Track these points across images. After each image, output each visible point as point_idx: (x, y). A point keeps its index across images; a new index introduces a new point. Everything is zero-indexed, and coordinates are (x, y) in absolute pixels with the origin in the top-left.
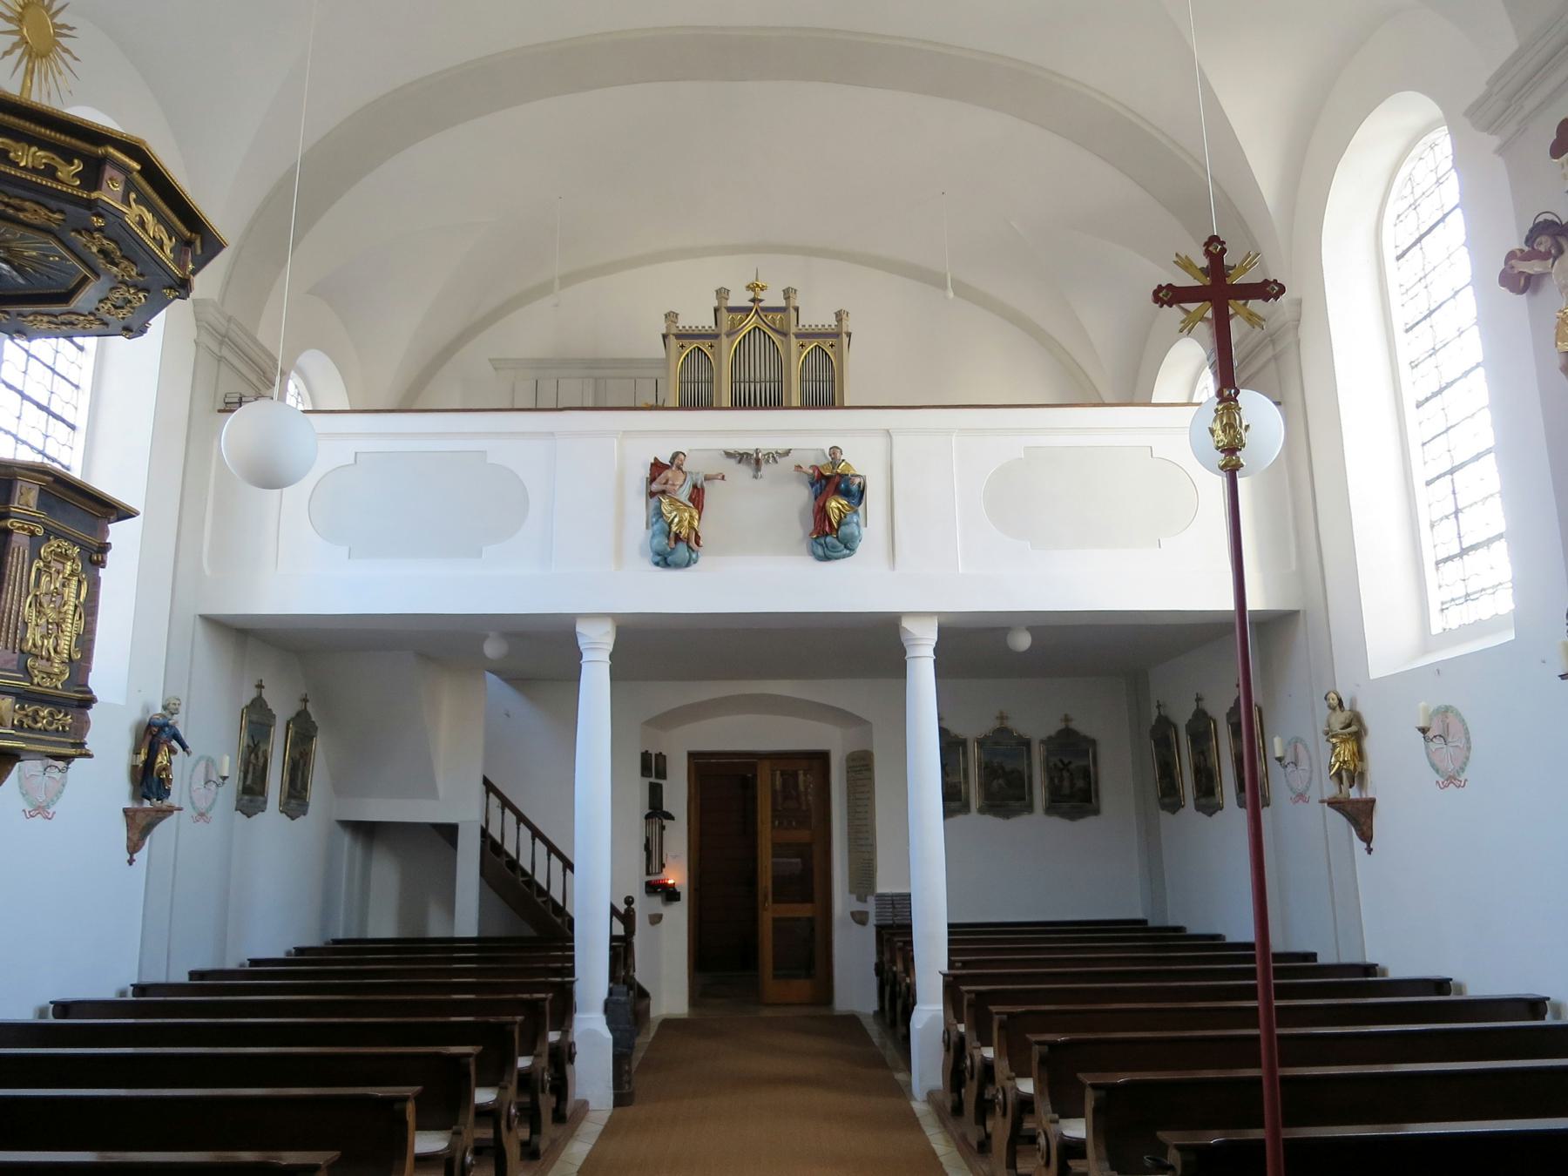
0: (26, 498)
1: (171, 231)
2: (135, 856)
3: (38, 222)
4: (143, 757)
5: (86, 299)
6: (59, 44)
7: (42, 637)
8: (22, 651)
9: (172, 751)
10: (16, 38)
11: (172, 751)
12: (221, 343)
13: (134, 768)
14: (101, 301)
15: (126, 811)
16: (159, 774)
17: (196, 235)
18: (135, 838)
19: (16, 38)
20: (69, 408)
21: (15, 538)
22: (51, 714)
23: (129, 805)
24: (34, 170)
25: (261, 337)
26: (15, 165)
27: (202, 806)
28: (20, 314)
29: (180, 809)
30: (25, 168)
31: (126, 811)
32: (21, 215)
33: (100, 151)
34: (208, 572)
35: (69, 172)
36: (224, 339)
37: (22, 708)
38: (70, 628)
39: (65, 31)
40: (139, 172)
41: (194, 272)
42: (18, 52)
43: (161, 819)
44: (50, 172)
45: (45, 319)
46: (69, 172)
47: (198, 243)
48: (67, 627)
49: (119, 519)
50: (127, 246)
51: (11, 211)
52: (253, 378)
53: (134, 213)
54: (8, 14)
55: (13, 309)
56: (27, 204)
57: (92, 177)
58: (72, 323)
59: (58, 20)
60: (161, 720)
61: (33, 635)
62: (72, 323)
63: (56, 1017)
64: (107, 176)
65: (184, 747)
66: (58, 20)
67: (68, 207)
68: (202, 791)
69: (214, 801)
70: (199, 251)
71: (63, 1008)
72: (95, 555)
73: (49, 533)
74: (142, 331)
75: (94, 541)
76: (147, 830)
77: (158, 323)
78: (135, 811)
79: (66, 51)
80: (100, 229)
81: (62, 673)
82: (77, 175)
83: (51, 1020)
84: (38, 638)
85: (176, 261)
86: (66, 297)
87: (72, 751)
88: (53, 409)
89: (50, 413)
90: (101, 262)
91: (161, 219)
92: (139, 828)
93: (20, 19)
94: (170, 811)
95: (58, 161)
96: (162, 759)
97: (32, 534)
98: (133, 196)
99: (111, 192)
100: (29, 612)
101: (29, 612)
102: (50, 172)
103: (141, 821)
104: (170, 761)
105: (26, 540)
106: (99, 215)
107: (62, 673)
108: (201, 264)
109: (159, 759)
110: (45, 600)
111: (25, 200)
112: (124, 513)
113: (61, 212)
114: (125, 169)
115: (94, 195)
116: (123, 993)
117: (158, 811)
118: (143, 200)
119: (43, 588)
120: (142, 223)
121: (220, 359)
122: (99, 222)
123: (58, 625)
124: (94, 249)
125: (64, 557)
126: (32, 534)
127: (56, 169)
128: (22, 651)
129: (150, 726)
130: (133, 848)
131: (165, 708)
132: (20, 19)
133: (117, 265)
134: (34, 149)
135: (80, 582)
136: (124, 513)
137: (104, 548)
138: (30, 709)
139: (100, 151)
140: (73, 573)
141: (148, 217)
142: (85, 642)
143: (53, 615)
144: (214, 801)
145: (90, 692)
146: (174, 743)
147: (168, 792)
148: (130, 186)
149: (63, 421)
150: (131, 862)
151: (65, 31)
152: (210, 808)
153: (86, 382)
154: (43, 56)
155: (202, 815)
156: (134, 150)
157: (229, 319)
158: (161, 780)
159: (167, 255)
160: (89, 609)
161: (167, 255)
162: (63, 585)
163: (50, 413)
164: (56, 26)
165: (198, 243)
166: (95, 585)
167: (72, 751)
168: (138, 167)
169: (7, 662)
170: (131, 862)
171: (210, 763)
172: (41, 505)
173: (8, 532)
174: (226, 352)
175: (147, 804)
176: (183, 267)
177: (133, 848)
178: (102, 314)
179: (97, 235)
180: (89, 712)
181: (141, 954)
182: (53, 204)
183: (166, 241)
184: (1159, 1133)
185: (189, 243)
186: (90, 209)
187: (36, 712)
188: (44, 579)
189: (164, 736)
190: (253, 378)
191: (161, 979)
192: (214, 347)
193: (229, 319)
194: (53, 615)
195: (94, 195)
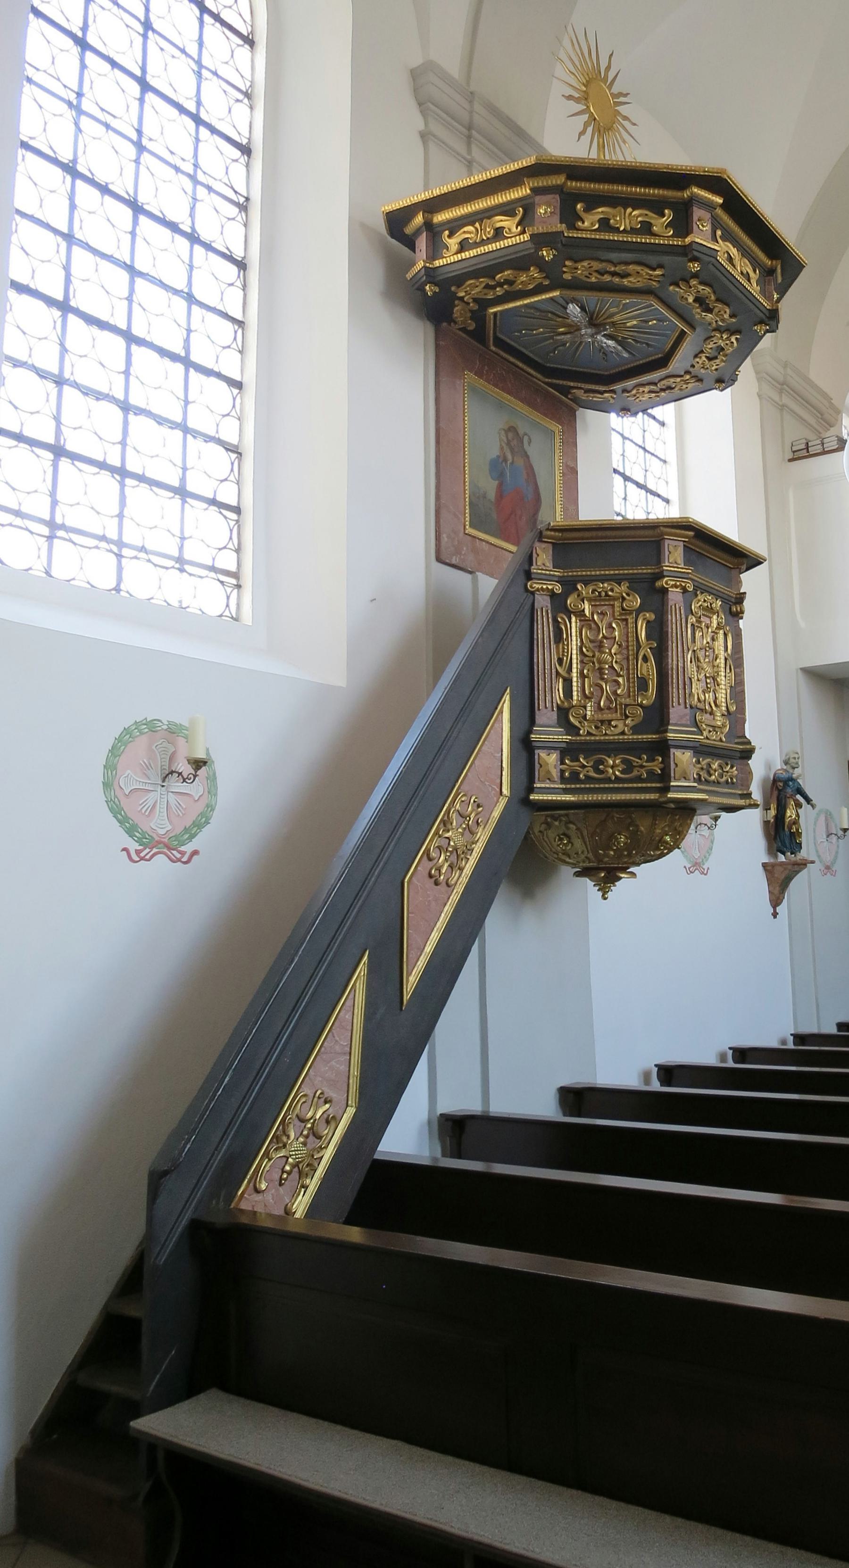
0: (674, 556)
1: (755, 263)
2: (778, 909)
3: (639, 285)
4: (773, 812)
5: (677, 364)
6: (618, 113)
7: (704, 692)
8: (691, 707)
9: (798, 805)
10: (585, 117)
11: (798, 805)
12: (781, 392)
13: (766, 823)
14: (696, 356)
15: (764, 865)
16: (790, 828)
17: (777, 258)
18: (776, 891)
19: (585, 117)
20: (662, 483)
21: (671, 596)
22: (720, 766)
23: (766, 859)
24: (633, 231)
25: (813, 376)
26: (617, 230)
27: (828, 858)
28: (625, 391)
29: (813, 862)
30: (624, 231)
31: (764, 865)
32: (625, 282)
33: (686, 194)
34: (802, 624)
35: (661, 223)
36: (782, 386)
37: (698, 762)
38: (724, 680)
39: (622, 99)
40: (722, 206)
41: (779, 300)
42: (590, 130)
43: (797, 872)
44: (646, 228)
45: (646, 389)
46: (661, 223)
47: (779, 271)
48: (722, 679)
49: (748, 569)
50: (725, 290)
51: (617, 280)
52: (812, 421)
53: (723, 248)
54: (577, 95)
55: (618, 387)
56: (632, 268)
57: (682, 225)
58: (670, 388)
59: (615, 89)
60: (785, 775)
61: (697, 688)
62: (670, 388)
63: (735, 1062)
64: (695, 218)
65: (808, 800)
66: (615, 89)
67: (666, 259)
68: (826, 843)
69: (837, 853)
70: (780, 280)
71: (741, 1054)
72: (734, 606)
73: (699, 588)
74: (733, 380)
75: (731, 592)
76: (785, 884)
77: (746, 369)
78: (773, 865)
79: (626, 118)
80: (695, 276)
81: (724, 726)
82: (669, 225)
83: (730, 1064)
84: (700, 692)
85: (763, 292)
86: (663, 362)
87: (741, 802)
88: (651, 486)
89: (648, 491)
90: (697, 312)
91: (745, 253)
92: (779, 882)
93: (585, 98)
94: (803, 864)
95: (652, 217)
96: (790, 813)
97: (685, 590)
98: (719, 233)
99: (701, 235)
100: (691, 668)
101: (691, 668)
102: (646, 228)
103: (780, 874)
104: (798, 815)
105: (680, 597)
106: (695, 259)
107: (724, 726)
108: (783, 290)
109: (788, 813)
110: (701, 654)
111: (627, 263)
112: (754, 561)
113: (660, 266)
114: (709, 206)
115: (688, 240)
116: (784, 1042)
117: (796, 864)
118: (728, 237)
119: (698, 644)
120: (730, 259)
121: (782, 407)
122: (695, 267)
123: (714, 679)
124: (691, 300)
125: (710, 610)
126: (685, 590)
127: (650, 225)
128: (691, 707)
129: (775, 781)
130: (776, 902)
131: (786, 763)
132: (585, 98)
133: (710, 311)
134: (629, 210)
135: (725, 635)
136: (754, 561)
137: (740, 599)
138: (704, 762)
139: (686, 194)
140: (719, 627)
141: (734, 252)
142: (738, 693)
143: (709, 670)
144: (837, 853)
145: (749, 743)
146: (799, 797)
147: (800, 845)
148: (716, 224)
149: (659, 496)
150: (775, 915)
151: (622, 99)
152: (834, 861)
153: (671, 456)
154: (609, 130)
155: (828, 868)
156: (717, 183)
157: (785, 365)
158: (792, 835)
159: (754, 288)
160: (736, 660)
161: (754, 288)
162: (713, 639)
163: (648, 491)
164: (615, 96)
165: (779, 271)
166: (738, 635)
167: (741, 802)
168: (720, 200)
169: (681, 717)
170: (775, 915)
171: (829, 816)
172: (688, 562)
173: (664, 591)
174: (786, 400)
175: (782, 858)
176: (769, 298)
177: (776, 902)
178: (699, 371)
179: (693, 282)
180: (750, 762)
181: (794, 1004)
182: (653, 260)
183: (752, 274)
184: (133, 1424)
185: (771, 272)
186: (686, 255)
187: (709, 765)
188: (698, 634)
189: (789, 790)
190: (812, 421)
191: (814, 1030)
192: (776, 398)
193: (785, 365)
194: (709, 670)
195: (688, 240)
